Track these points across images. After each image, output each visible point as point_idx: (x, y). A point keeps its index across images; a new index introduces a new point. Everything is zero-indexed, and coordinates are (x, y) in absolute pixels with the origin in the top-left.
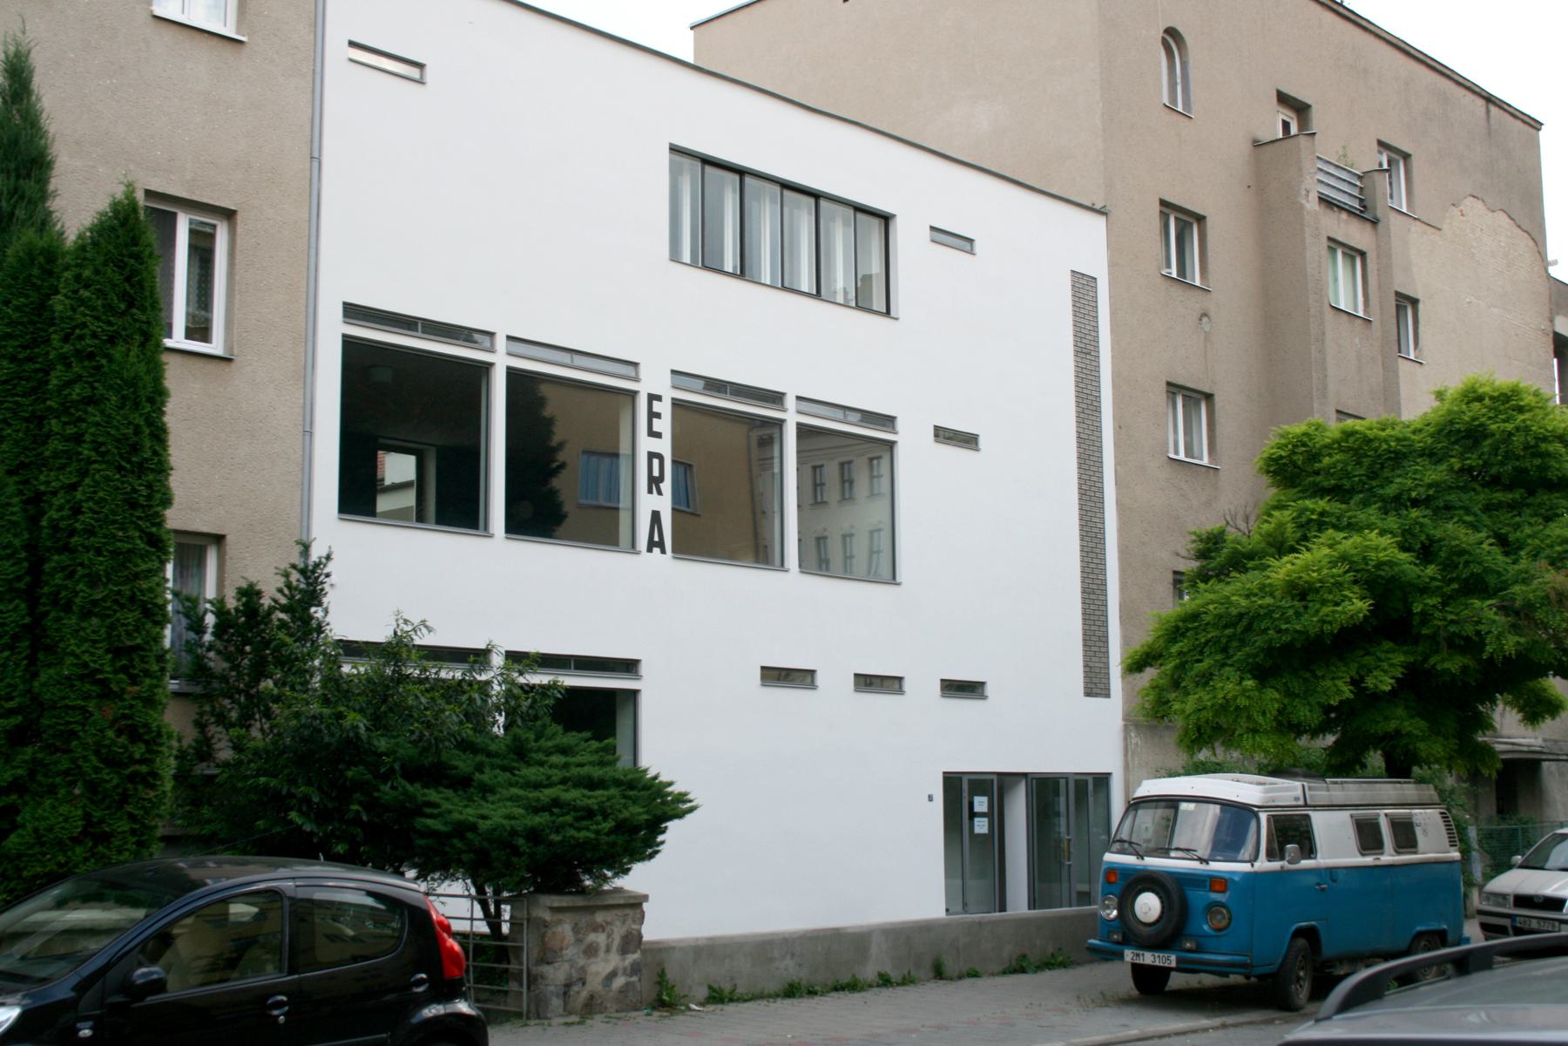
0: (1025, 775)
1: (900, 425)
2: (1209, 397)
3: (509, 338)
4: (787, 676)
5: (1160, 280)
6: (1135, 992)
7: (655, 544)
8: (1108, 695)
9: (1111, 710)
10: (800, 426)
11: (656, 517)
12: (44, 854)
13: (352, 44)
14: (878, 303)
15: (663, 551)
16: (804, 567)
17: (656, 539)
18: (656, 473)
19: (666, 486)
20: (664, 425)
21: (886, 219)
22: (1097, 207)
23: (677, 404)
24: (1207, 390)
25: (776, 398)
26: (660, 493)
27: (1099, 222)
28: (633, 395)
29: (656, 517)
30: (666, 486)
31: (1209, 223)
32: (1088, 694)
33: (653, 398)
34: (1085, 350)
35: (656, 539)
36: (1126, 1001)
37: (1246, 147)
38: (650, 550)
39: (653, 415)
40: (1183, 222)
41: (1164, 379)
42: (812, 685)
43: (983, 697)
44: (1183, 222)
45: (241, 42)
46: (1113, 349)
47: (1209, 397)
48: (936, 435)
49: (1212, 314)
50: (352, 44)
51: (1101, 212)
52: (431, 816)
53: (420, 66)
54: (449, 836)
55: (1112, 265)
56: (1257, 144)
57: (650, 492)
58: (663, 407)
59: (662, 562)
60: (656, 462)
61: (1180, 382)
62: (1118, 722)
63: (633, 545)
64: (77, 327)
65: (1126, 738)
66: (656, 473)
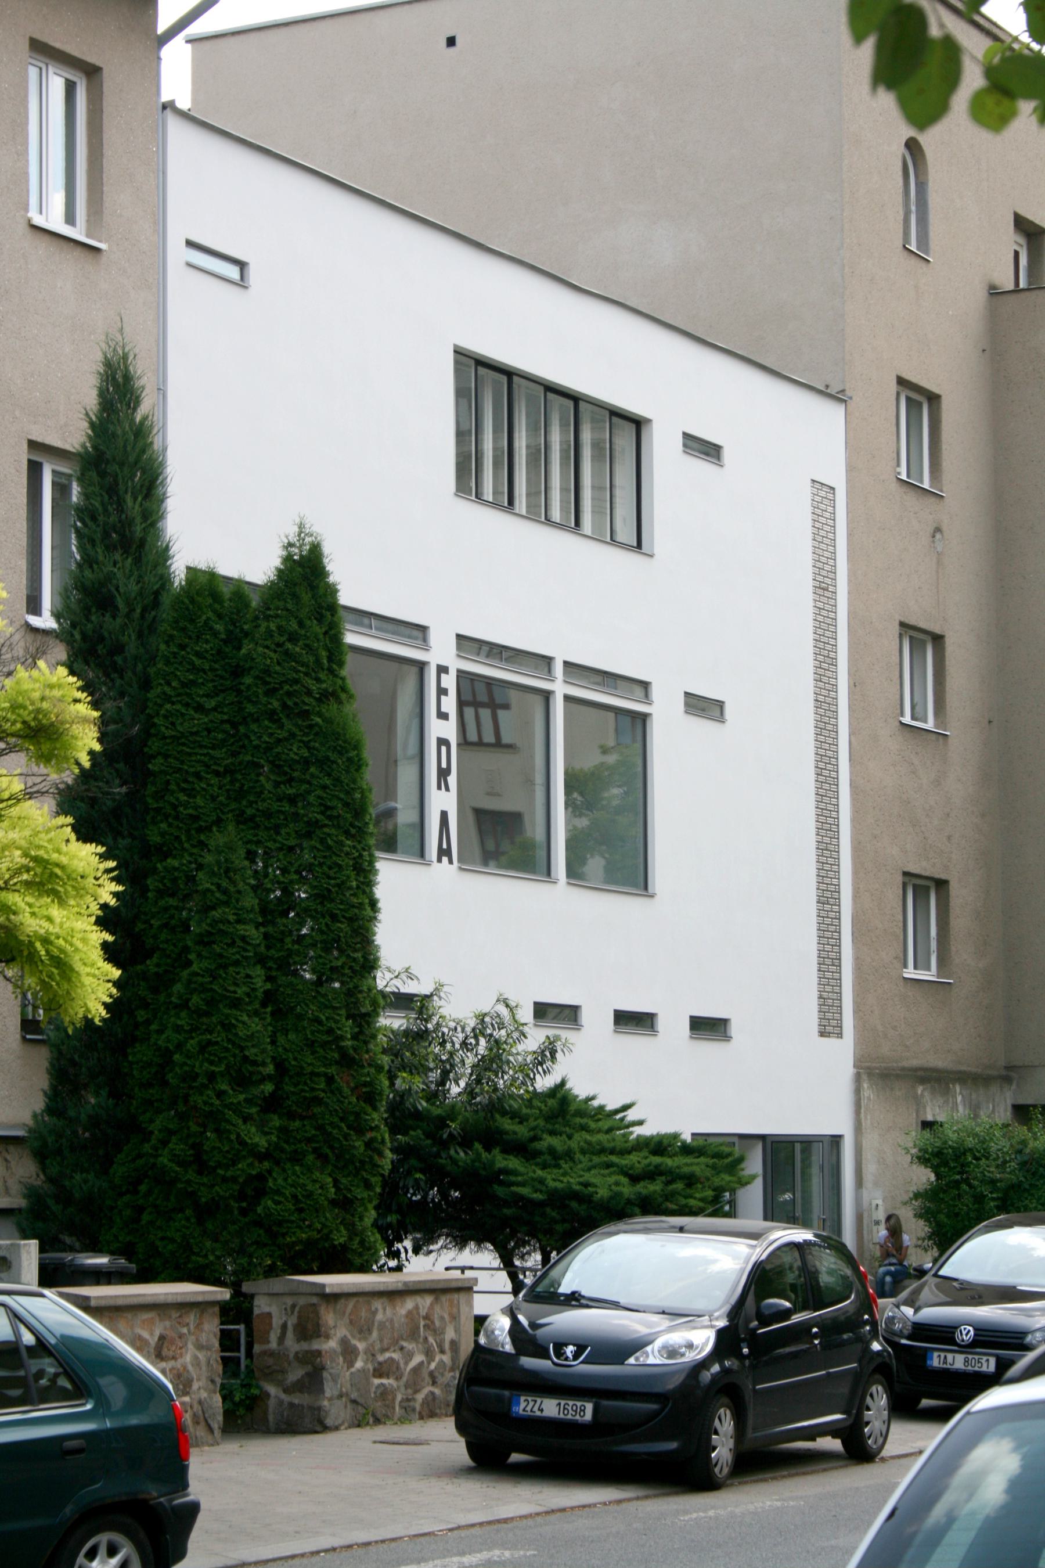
0: (763, 1138)
1: (655, 692)
2: (938, 640)
3: (566, 664)
4: (714, 1025)
5: (894, 486)
6: (470, 1462)
7: (444, 852)
8: (840, 1035)
9: (840, 1055)
10: (567, 698)
11: (444, 815)
12: (304, 1220)
13: (190, 244)
14: (626, 533)
15: (451, 862)
16: (574, 873)
17: (445, 846)
18: (444, 765)
19: (452, 780)
20: (450, 704)
21: (638, 424)
22: (832, 391)
23: (461, 674)
24: (937, 630)
25: (419, 632)
26: (447, 789)
27: (834, 415)
28: (421, 666)
29: (444, 815)
30: (452, 780)
31: (946, 404)
32: (822, 1034)
33: (442, 670)
34: (824, 589)
35: (445, 846)
36: (468, 1471)
37: (982, 295)
38: (439, 860)
39: (442, 692)
40: (919, 400)
41: (898, 618)
42: (726, 1037)
43: (726, 1037)
44: (919, 400)
45: (97, 250)
46: (850, 581)
47: (938, 640)
48: (459, 647)
49: (944, 528)
50: (190, 244)
51: (838, 397)
52: (519, 1184)
53: (242, 265)
54: (541, 1204)
55: (850, 468)
56: (994, 292)
57: (439, 788)
58: (449, 681)
59: (445, 872)
60: (444, 749)
61: (912, 621)
62: (847, 1070)
63: (422, 854)
64: (286, 682)
65: (858, 1091)
66: (444, 765)
